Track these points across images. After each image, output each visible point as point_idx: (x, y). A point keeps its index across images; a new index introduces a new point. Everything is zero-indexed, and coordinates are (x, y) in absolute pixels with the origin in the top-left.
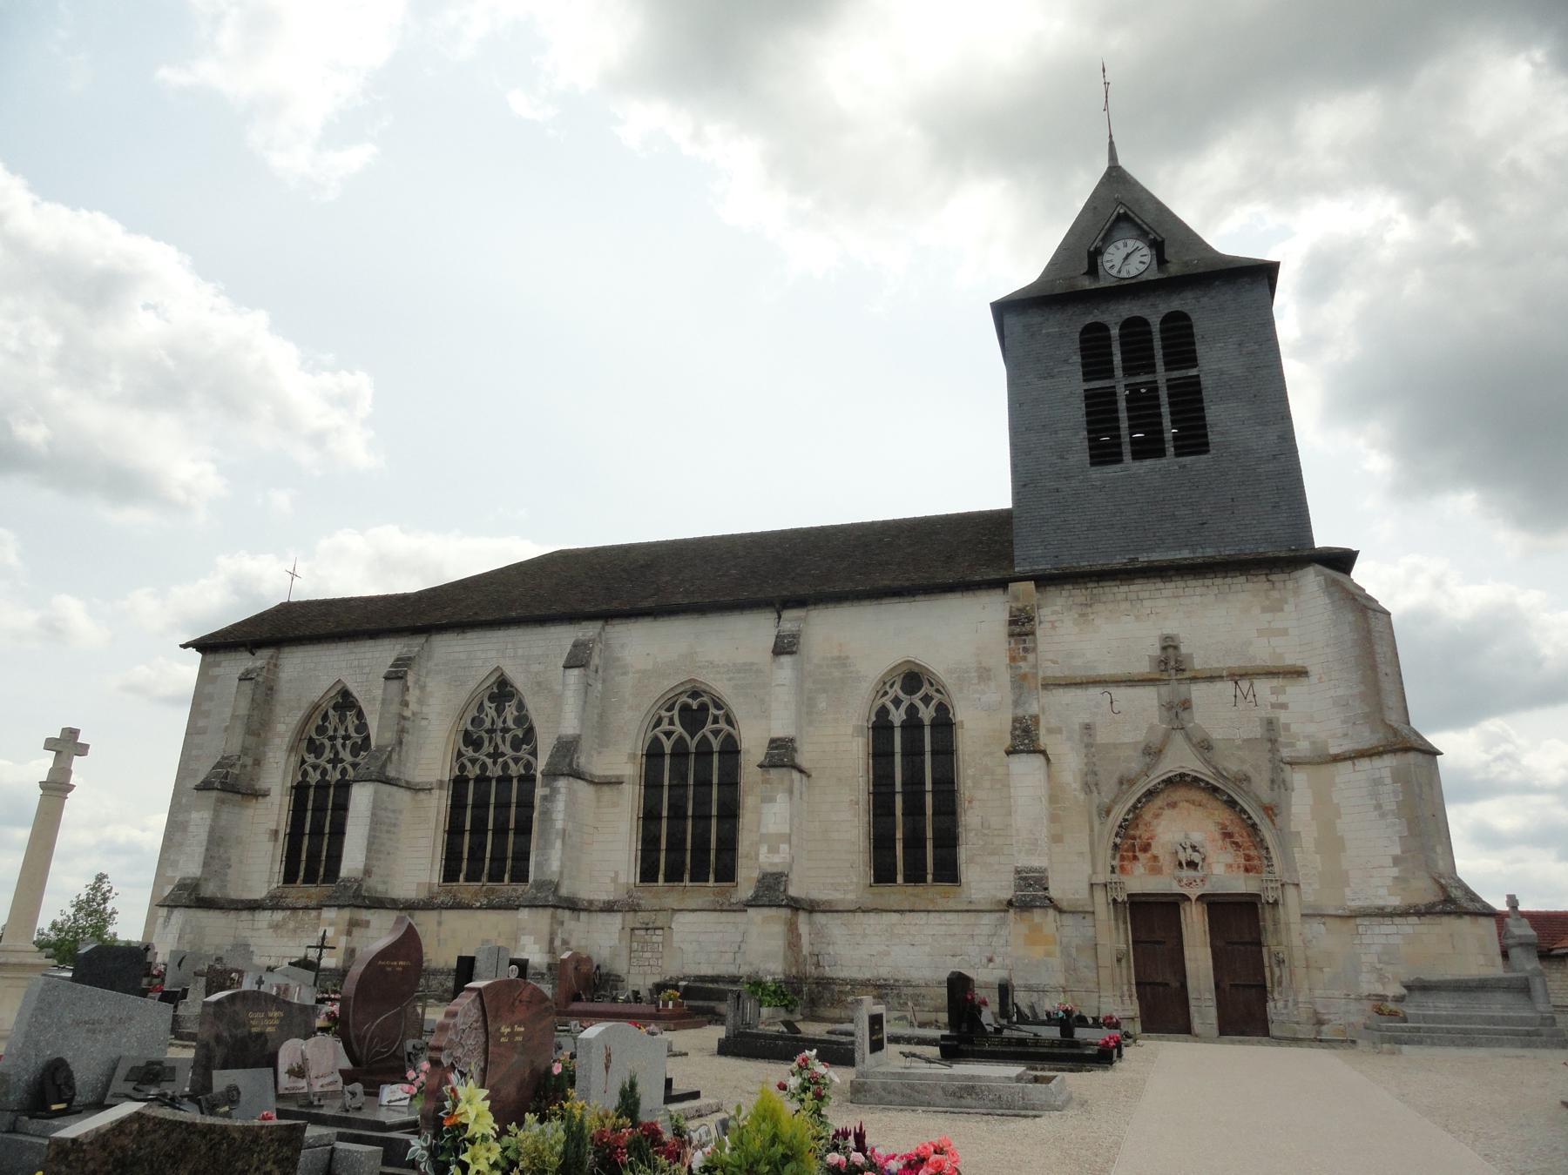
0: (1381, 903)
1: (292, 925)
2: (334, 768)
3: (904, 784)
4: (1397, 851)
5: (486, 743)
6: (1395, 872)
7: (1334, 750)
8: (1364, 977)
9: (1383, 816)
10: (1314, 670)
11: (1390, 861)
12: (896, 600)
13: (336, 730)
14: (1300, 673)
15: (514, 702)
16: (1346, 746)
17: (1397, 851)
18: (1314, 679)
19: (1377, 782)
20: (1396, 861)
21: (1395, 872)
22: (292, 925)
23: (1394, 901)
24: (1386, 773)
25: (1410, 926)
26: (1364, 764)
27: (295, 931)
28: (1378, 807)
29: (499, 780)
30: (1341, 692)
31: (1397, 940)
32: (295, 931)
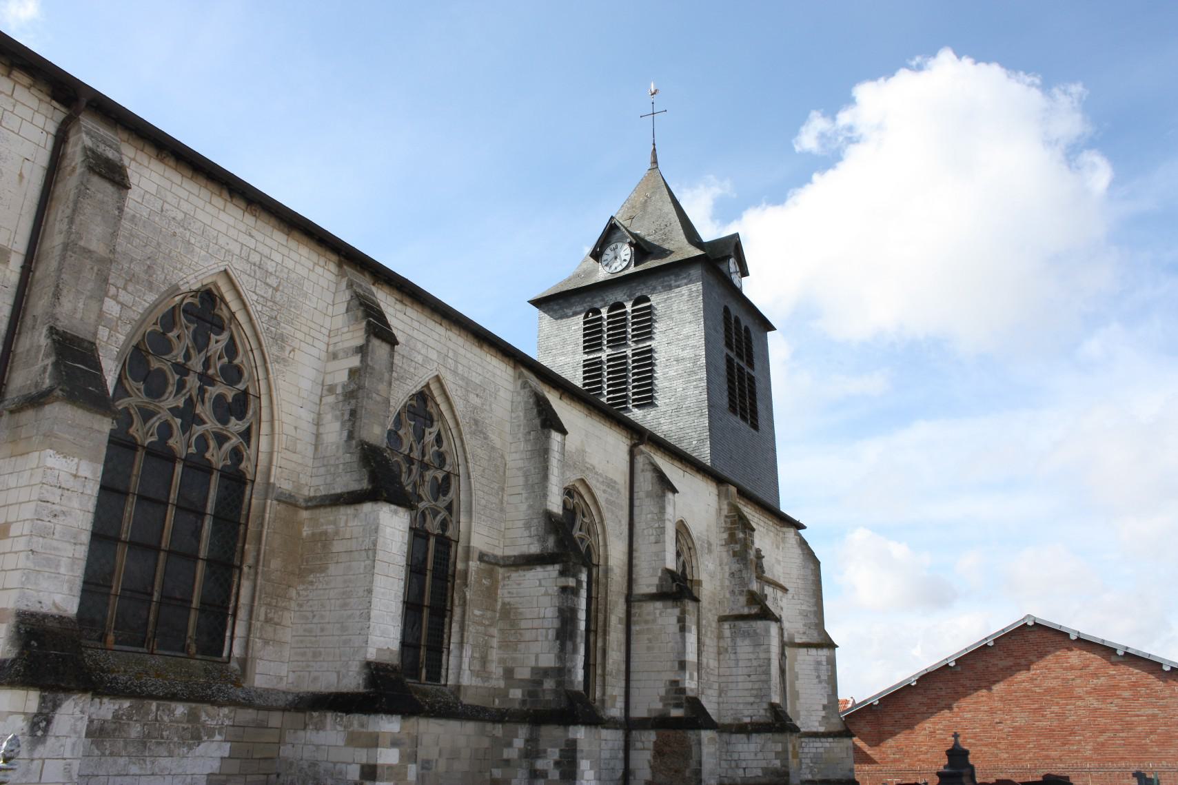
0: (814, 730)
1: (135, 730)
2: (185, 428)
3: (218, 503)
4: (825, 702)
5: (171, 389)
6: (823, 713)
7: (797, 641)
8: (803, 771)
9: (820, 682)
10: (791, 591)
11: (821, 707)
12: (305, 239)
13: (187, 357)
14: (785, 590)
15: (224, 337)
16: (804, 639)
17: (825, 702)
18: (789, 596)
19: (819, 663)
20: (825, 707)
21: (823, 713)
22: (135, 730)
23: (822, 729)
24: (824, 659)
25: (828, 743)
26: (813, 651)
27: (143, 742)
28: (818, 677)
29: (151, 452)
30: (804, 607)
31: (822, 750)
32: (143, 742)
